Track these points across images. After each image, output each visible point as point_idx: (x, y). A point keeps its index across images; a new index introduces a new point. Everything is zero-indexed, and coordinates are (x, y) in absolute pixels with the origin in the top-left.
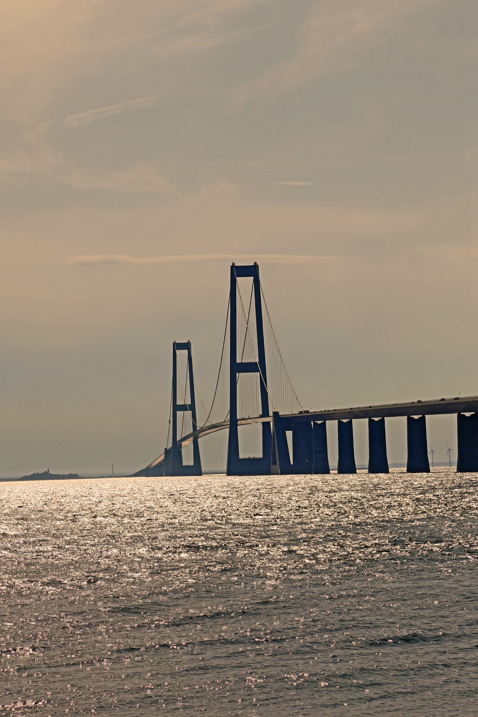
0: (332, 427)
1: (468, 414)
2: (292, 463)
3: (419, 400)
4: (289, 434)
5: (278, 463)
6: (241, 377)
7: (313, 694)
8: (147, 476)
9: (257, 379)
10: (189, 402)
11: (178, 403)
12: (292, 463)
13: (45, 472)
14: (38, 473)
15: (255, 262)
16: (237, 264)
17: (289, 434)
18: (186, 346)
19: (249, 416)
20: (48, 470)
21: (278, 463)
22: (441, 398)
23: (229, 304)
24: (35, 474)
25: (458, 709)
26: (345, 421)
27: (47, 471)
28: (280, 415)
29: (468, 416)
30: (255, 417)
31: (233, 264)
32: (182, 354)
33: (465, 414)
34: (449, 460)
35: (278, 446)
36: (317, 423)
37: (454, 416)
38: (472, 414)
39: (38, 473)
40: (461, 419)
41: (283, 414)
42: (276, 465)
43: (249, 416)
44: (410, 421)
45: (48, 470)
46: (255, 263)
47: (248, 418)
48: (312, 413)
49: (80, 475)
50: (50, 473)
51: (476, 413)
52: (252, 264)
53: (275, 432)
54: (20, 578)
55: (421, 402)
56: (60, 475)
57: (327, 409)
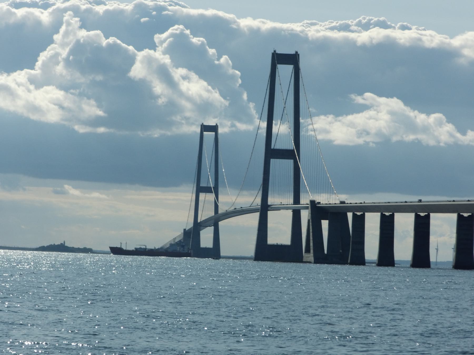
0: (350, 215)
1: (466, 215)
2: (326, 252)
4: (325, 224)
5: (312, 251)
6: (274, 162)
9: (275, 171)
10: (212, 185)
12: (326, 252)
13: (62, 244)
14: (54, 244)
15: (297, 51)
16: (278, 52)
17: (325, 224)
18: (214, 129)
19: (281, 203)
20: (64, 242)
21: (312, 251)
23: (292, 73)
24: (51, 245)
25: (253, 336)
27: (63, 243)
29: (359, 214)
31: (275, 51)
32: (209, 135)
33: (420, 214)
35: (313, 235)
36: (356, 214)
37: (379, 214)
38: (390, 214)
39: (54, 244)
40: (460, 218)
41: (334, 203)
42: (310, 253)
43: (281, 203)
44: (383, 216)
45: (64, 242)
47: (280, 204)
49: (94, 249)
50: (66, 245)
51: (473, 214)
53: (311, 220)
54: (77, 258)
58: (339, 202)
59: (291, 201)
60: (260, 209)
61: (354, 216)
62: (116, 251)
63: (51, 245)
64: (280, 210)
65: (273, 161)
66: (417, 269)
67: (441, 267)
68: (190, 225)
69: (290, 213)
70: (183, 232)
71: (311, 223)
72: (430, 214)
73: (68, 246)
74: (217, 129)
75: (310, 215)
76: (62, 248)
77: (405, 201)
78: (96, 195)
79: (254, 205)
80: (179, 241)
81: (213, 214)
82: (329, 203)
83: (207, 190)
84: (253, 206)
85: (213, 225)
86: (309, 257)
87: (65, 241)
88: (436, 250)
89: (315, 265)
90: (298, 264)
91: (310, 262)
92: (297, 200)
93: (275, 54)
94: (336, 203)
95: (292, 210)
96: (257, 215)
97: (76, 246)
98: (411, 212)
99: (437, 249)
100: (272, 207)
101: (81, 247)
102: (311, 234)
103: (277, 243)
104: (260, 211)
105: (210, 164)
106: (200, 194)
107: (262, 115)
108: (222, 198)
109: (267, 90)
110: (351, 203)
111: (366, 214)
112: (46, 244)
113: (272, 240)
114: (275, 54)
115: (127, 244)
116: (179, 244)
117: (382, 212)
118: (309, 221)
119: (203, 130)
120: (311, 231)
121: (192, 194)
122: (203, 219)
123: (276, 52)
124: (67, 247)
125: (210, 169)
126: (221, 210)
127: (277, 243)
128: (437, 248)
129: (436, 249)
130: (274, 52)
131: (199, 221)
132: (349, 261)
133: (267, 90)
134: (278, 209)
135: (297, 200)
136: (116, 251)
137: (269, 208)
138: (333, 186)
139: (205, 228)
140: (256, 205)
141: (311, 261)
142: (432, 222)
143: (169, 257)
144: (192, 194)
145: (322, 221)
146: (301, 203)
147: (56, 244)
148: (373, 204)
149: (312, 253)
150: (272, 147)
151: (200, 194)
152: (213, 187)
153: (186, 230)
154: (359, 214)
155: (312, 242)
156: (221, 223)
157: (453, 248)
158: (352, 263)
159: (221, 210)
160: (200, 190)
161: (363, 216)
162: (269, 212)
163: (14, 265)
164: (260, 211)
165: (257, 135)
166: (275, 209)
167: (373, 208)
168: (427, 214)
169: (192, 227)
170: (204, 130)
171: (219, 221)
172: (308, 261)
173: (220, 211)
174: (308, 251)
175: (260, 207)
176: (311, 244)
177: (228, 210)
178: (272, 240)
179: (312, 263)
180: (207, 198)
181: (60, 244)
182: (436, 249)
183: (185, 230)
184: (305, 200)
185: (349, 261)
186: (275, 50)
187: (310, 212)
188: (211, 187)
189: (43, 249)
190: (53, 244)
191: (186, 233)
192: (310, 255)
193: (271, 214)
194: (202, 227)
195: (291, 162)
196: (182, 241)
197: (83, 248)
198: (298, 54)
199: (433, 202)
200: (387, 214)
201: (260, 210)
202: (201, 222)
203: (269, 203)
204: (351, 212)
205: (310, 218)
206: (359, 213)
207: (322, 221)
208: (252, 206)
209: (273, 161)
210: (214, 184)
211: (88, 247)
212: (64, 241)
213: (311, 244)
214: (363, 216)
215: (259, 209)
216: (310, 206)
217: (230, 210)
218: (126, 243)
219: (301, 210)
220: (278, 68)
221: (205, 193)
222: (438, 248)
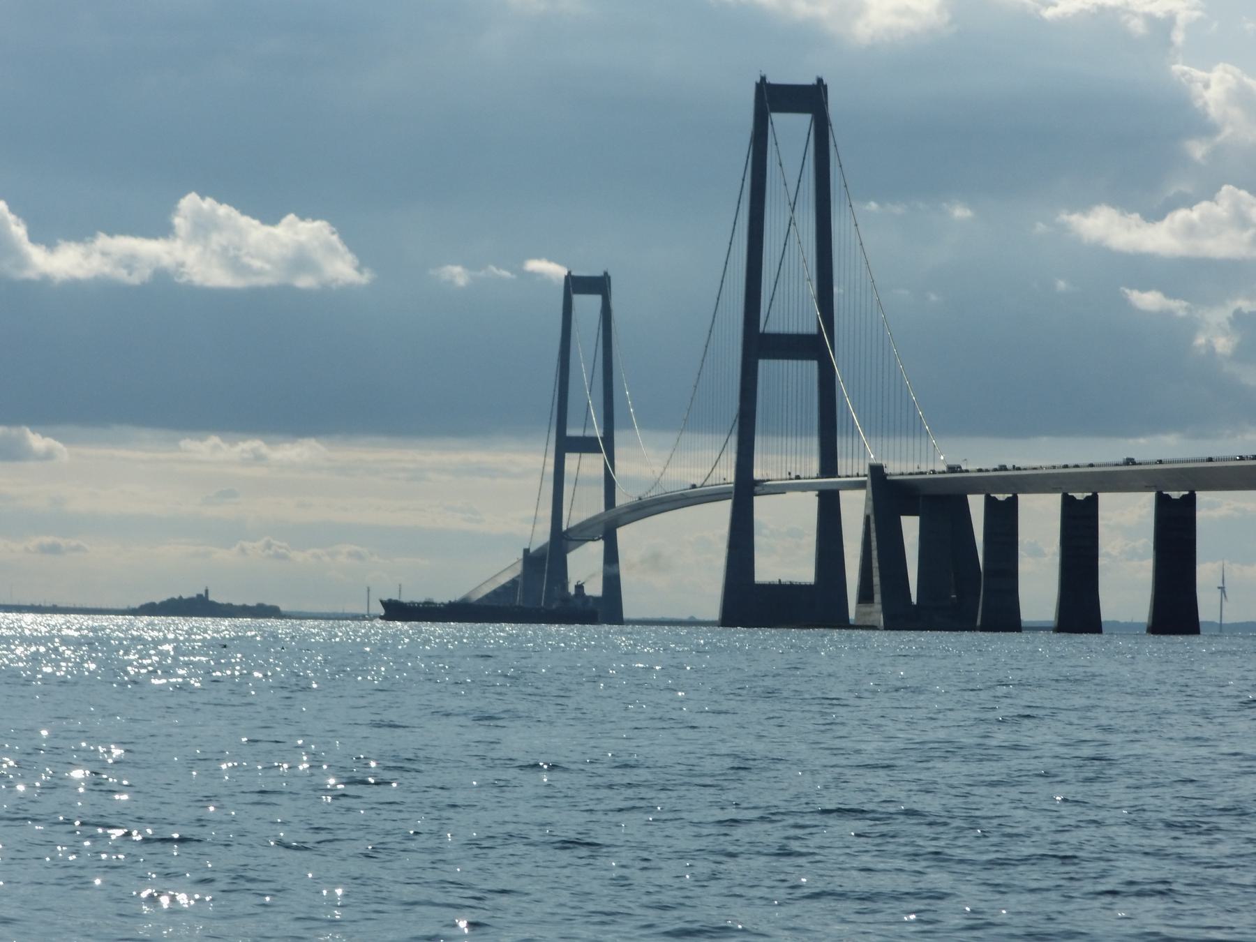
2: (914, 599)
3: (1130, 456)
4: (911, 526)
5: (877, 597)
6: (766, 367)
7: (827, 925)
8: (614, 459)
10: (598, 433)
11: (572, 432)
12: (914, 599)
13: (199, 596)
14: (181, 597)
16: (771, 80)
17: (911, 526)
18: (599, 285)
19: (790, 474)
20: (207, 591)
21: (877, 597)
22: (978, 468)
23: (809, 134)
26: (1001, 497)
28: (887, 475)
30: (718, 482)
31: (763, 79)
32: (588, 305)
33: (1170, 493)
34: (577, 489)
39: (181, 597)
42: (873, 602)
44: (1068, 502)
45: (207, 591)
46: (820, 81)
48: (987, 471)
49: (284, 608)
52: (811, 81)
53: (872, 518)
55: (1134, 463)
56: (236, 606)
57: (1071, 462)
58: (945, 469)
59: (814, 466)
60: (733, 492)
61: (990, 503)
62: (396, 610)
63: (172, 601)
64: (785, 493)
65: (763, 365)
66: (1164, 638)
67: (1125, 629)
68: (541, 536)
69: (809, 503)
70: (521, 556)
71: (873, 526)
72: (1017, 497)
73: (217, 601)
74: (607, 283)
75: (871, 503)
76: (200, 606)
77: (1064, 464)
78: (1142, 441)
79: (709, 482)
80: (511, 580)
81: (602, 509)
82: (919, 471)
83: (586, 445)
84: (708, 486)
85: (601, 536)
86: (870, 614)
87: (209, 589)
88: (1220, 590)
89: (887, 633)
90: (1084, 637)
91: (873, 628)
92: (829, 464)
93: (764, 86)
94: (937, 469)
95: (817, 492)
96: (725, 507)
97: (237, 602)
98: (1147, 489)
99: (1222, 589)
100: (770, 485)
101: (252, 603)
102: (875, 553)
103: (780, 581)
104: (735, 496)
105: (590, 381)
106: (567, 455)
107: (732, 245)
108: (623, 469)
109: (743, 180)
110: (1077, 466)
111: (1021, 497)
112: (158, 599)
113: (768, 569)
114: (764, 86)
115: (371, 593)
116: (507, 590)
117: (1160, 490)
118: (867, 519)
119: (571, 289)
120: (874, 544)
121: (545, 457)
122: (573, 523)
123: (767, 81)
124: (213, 603)
125: (590, 391)
126: (623, 498)
127: (780, 581)
128: (1221, 585)
129: (1219, 588)
130: (761, 81)
131: (564, 528)
132: (979, 622)
133: (743, 180)
134: (780, 490)
135: (829, 464)
136: (396, 610)
137: (757, 489)
138: (927, 428)
139: (581, 545)
140: (722, 481)
141: (876, 624)
142: (1201, 514)
143: (245, 619)
144: (545, 457)
145: (902, 517)
146: (839, 474)
147: (185, 596)
148: (1090, 469)
149: (878, 603)
150: (761, 330)
151: (567, 455)
152: (601, 438)
153: (531, 551)
154: (1003, 497)
155: (878, 574)
156: (623, 534)
157: (782, 581)
158: (984, 628)
159: (623, 498)
160: (566, 445)
161: (1013, 502)
162: (756, 499)
163: (32, 653)
164: (733, 498)
165: (720, 298)
166: (773, 491)
167: (1039, 483)
168: (1187, 493)
169: (546, 544)
170: (573, 289)
171: (618, 527)
172: (869, 624)
173: (621, 500)
174: (865, 596)
175: (732, 485)
176: (876, 580)
177: (644, 495)
178: (768, 569)
179: (878, 629)
180: (584, 470)
181: (195, 596)
182: (1219, 588)
183: (526, 551)
184: (852, 464)
185: (979, 622)
186: (763, 75)
187: (870, 495)
188: (597, 438)
189: (151, 609)
190: (176, 597)
191: (531, 560)
192: (872, 609)
193: (762, 506)
194: (571, 544)
195: (812, 367)
196: (520, 580)
197: (255, 605)
198: (824, 83)
199: (1188, 461)
200: (1079, 496)
201: (733, 495)
202: (569, 530)
203: (757, 474)
204: (1058, 492)
205: (870, 511)
206: (1080, 494)
207: (902, 517)
208: (706, 484)
209: (763, 365)
210: (602, 431)
211: (268, 602)
212: (207, 587)
213: (876, 580)
214: (1012, 504)
215: (731, 493)
216: (870, 478)
217: (651, 495)
218: (369, 591)
219: (840, 492)
220: (772, 123)
221: (578, 455)
222: (1225, 585)
